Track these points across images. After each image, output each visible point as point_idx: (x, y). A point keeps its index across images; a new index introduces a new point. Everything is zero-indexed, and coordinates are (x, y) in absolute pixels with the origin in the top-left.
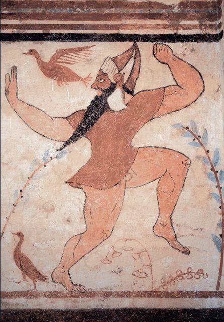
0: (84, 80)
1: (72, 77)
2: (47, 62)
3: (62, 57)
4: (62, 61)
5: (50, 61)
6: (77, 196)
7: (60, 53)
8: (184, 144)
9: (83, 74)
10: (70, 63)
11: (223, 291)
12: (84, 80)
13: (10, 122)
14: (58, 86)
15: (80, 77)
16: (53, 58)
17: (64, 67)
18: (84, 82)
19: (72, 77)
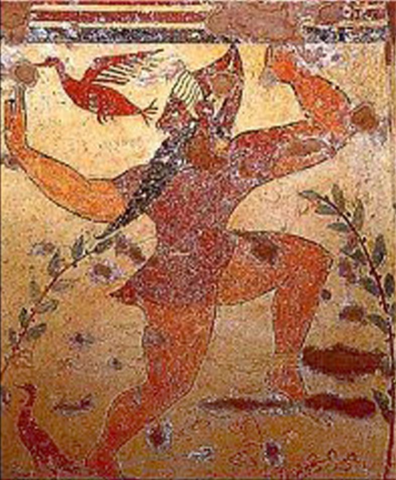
0: (144, 113)
1: (125, 108)
2: (79, 79)
3: (105, 72)
4: (103, 77)
5: (84, 79)
6: (135, 315)
7: (104, 62)
8: (313, 227)
9: (142, 103)
10: (118, 83)
11: (393, 3)
12: (144, 113)
13: (380, 222)
14: (100, 125)
15: (137, 108)
16: (89, 73)
17: (108, 89)
18: (145, 117)
19: (125, 108)
